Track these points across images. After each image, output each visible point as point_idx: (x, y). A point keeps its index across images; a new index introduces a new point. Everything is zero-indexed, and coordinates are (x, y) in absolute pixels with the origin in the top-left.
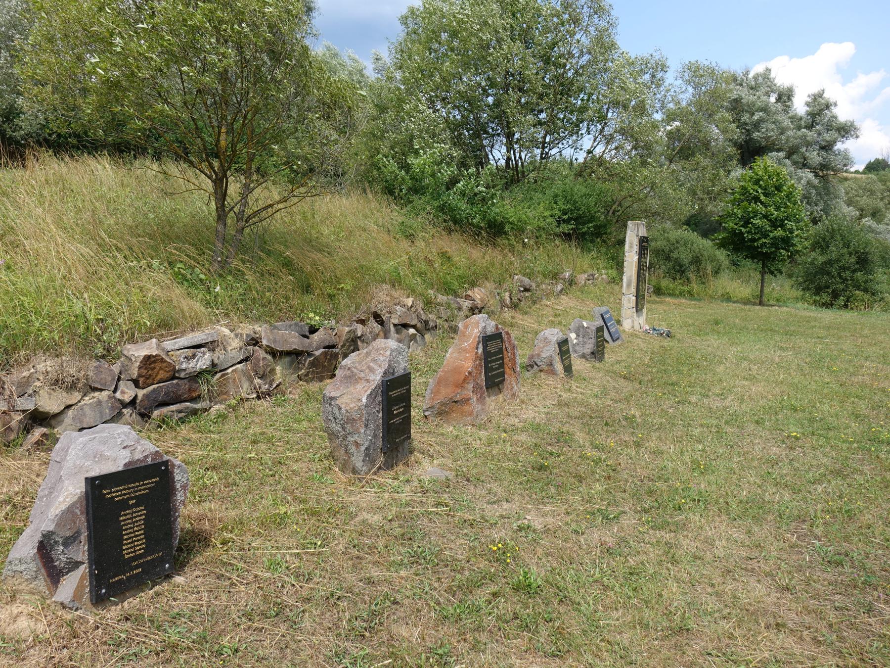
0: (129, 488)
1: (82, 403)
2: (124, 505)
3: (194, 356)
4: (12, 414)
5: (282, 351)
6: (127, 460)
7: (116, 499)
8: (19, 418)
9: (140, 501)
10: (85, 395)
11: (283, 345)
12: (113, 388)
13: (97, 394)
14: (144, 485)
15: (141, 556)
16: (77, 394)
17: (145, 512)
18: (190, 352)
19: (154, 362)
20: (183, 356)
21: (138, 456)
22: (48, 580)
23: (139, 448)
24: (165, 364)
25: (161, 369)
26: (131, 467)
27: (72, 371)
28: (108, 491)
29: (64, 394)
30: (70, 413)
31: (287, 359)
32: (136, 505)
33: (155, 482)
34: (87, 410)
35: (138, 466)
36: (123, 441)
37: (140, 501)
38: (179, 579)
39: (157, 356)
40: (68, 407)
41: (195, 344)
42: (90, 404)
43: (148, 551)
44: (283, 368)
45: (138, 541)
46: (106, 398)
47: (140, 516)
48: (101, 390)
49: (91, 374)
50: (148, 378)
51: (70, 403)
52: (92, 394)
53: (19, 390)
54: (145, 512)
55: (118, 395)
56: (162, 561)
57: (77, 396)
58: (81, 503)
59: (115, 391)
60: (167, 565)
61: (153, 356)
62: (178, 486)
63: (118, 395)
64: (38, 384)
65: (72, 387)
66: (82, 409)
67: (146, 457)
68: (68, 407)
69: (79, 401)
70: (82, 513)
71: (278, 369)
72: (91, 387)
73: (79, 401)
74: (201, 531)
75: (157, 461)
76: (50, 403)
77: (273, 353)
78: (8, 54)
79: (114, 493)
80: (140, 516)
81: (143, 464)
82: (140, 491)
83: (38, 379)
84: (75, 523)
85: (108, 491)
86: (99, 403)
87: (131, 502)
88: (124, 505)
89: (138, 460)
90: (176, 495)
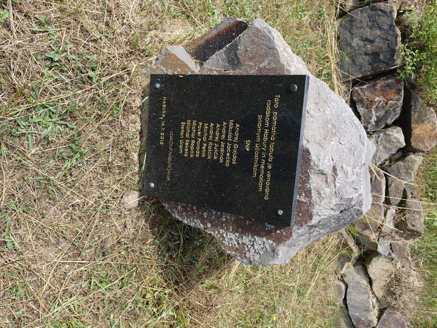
0: (268, 144)
1: (371, 296)
2: (248, 130)
4: (377, 234)
6: (313, 157)
7: (260, 117)
9: (245, 158)
10: (378, 300)
13: (376, 312)
14: (266, 170)
15: (176, 147)
17: (227, 165)
21: (315, 182)
22: (202, 42)
23: (328, 190)
27: (405, 297)
28: (276, 106)
29: (383, 283)
30: (364, 282)
32: (242, 154)
33: (263, 191)
34: (365, 297)
35: (298, 175)
36: (346, 173)
37: (245, 158)
38: (132, 199)
40: (370, 282)
42: (368, 302)
43: (178, 156)
45: (195, 146)
46: (370, 318)
47: (225, 156)
48: (379, 318)
49: (398, 315)
51: (375, 284)
52: (377, 308)
53: (397, 247)
54: (227, 165)
56: (159, 180)
57: (380, 293)
58: (274, 69)
60: (152, 185)
62: (246, 240)
64: (399, 265)
65: (390, 292)
66: (365, 293)
67: (308, 193)
68: (370, 282)
69: (373, 293)
70: (260, 69)
72: (385, 309)
73: (373, 293)
74: (190, 286)
75: (294, 212)
76: (378, 268)
79: (271, 113)
80: (225, 156)
81: (297, 185)
82: (260, 162)
83: (403, 267)
84: (251, 59)
85: (276, 106)
86: (368, 310)
87: (248, 143)
88: (248, 130)
89: (308, 177)
90: (234, 232)
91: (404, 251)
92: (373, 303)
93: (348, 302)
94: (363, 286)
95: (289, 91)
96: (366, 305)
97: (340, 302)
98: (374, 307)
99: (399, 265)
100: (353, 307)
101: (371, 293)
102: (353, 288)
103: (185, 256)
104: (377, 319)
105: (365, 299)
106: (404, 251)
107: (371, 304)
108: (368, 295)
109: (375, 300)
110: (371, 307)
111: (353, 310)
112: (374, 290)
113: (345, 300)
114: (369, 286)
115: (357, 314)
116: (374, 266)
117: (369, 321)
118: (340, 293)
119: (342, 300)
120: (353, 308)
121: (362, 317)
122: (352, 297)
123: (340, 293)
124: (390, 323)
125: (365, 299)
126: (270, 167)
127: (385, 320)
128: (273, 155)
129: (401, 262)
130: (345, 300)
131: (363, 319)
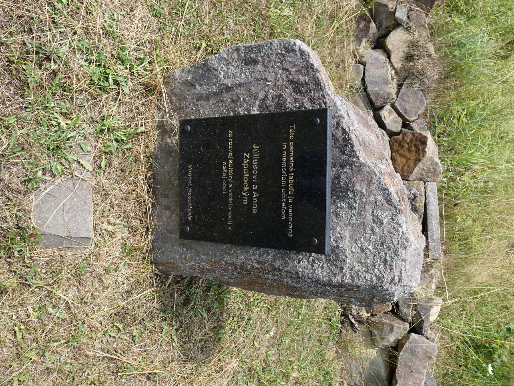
1: (390, 68)
3: (415, 209)
5: (396, 357)
8: (390, 6)
11: (406, 366)
12: (397, 105)
16: (400, 65)
18: (420, 204)
19: (418, 151)
20: (418, 193)
24: (412, 164)
25: (408, 159)
26: (331, 153)
30: (383, 57)
31: (383, 372)
39: (424, 152)
41: (429, 221)
44: (372, 363)
46: (388, 90)
50: (400, 144)
55: (388, 107)
59: (393, 106)
61: (424, 148)
63: (388, 107)
64: (417, 35)
69: (392, 65)
71: (373, 353)
73: (392, 65)
76: (396, 40)
77: (397, 347)
78: (42, 17)
91: (420, 18)
92: (391, 74)
93: (366, 79)
94: (382, 61)
95: (313, 124)
96: (385, 78)
97: (358, 83)
98: (393, 79)
99: (417, 35)
100: (371, 83)
101: (389, 66)
102: (372, 64)
103: (187, 301)
104: (396, 96)
105: (384, 72)
106: (420, 18)
107: (390, 76)
108: (387, 68)
109: (393, 72)
110: (390, 79)
111: (372, 85)
112: (392, 61)
113: (363, 80)
114: (388, 60)
115: (376, 89)
116: (392, 38)
117: (388, 93)
118: (358, 73)
119: (360, 80)
120: (372, 84)
121: (381, 91)
122: (371, 73)
123: (358, 73)
124: (409, 98)
125: (384, 72)
126: (291, 201)
127: (403, 94)
128: (294, 186)
129: (419, 32)
130: (363, 80)
131: (382, 93)
